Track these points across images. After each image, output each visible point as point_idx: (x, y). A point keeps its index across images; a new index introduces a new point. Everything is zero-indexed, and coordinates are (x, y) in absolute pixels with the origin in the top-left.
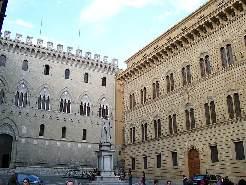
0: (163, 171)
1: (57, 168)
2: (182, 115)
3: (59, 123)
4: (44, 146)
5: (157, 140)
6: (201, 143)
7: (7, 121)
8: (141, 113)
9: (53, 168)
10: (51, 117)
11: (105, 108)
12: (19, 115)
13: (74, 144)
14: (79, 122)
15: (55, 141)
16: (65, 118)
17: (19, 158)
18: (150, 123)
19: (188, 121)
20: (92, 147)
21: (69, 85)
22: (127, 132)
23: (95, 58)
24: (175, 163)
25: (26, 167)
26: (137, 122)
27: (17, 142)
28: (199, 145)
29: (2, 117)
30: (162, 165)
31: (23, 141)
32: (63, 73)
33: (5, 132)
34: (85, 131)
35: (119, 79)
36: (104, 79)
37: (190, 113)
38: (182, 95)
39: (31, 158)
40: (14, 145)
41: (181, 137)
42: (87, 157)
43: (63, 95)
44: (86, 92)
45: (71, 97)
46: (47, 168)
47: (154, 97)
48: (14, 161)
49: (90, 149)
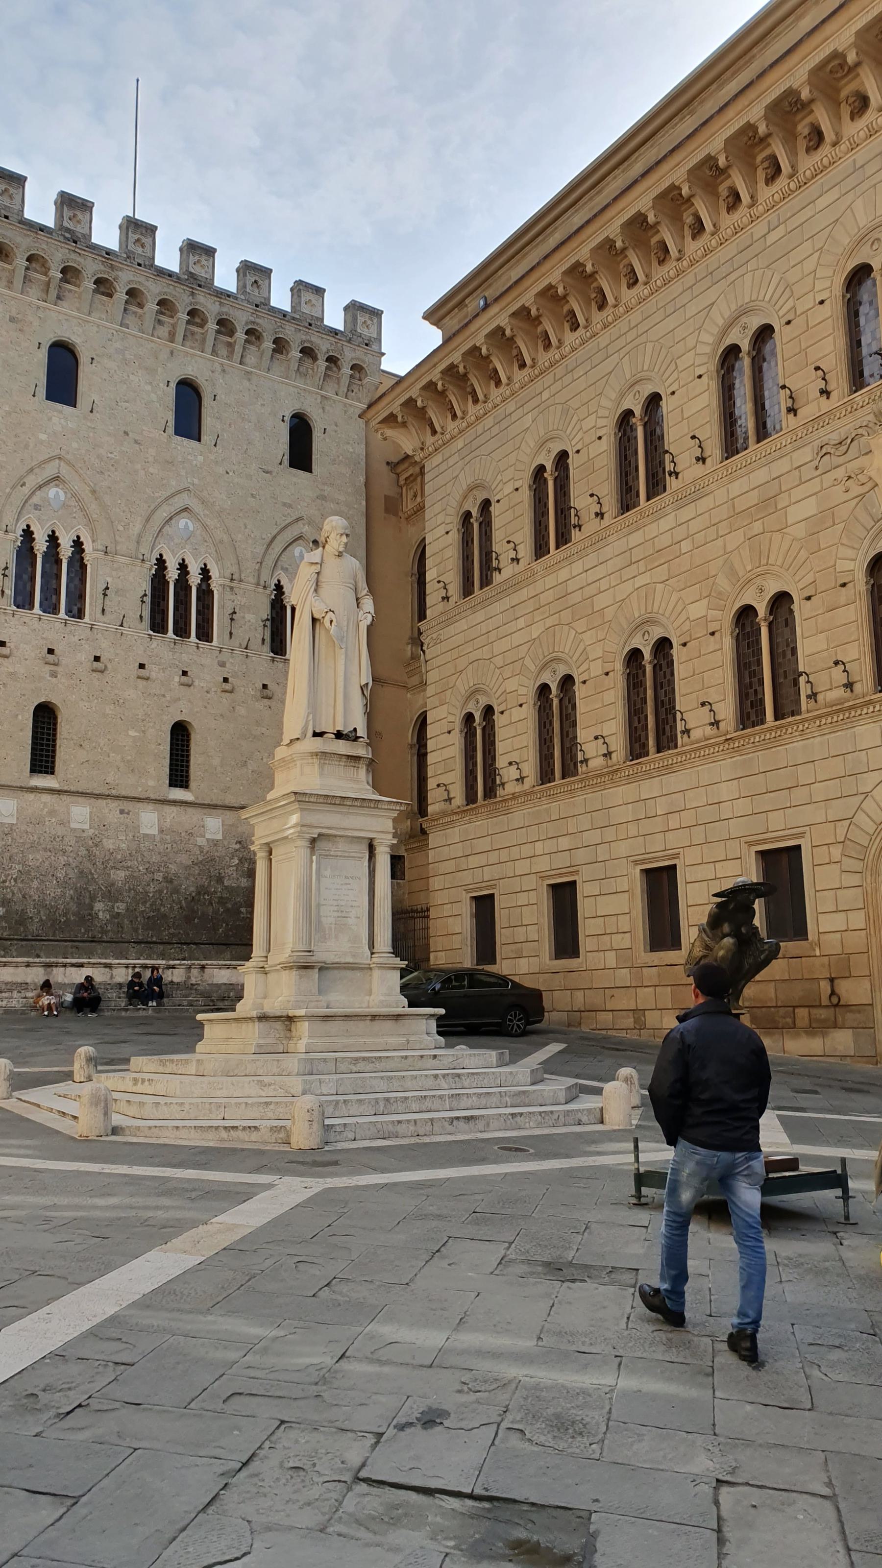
3: (12, 675)
13: (110, 811)
20: (228, 830)
21: (75, 445)
22: (445, 739)
23: (242, 287)
26: (507, 673)
32: (36, 368)
34: (180, 734)
35: (390, 419)
36: (301, 433)
38: (841, 460)
42: (199, 893)
43: (37, 507)
44: (185, 495)
45: (90, 522)
49: (215, 843)
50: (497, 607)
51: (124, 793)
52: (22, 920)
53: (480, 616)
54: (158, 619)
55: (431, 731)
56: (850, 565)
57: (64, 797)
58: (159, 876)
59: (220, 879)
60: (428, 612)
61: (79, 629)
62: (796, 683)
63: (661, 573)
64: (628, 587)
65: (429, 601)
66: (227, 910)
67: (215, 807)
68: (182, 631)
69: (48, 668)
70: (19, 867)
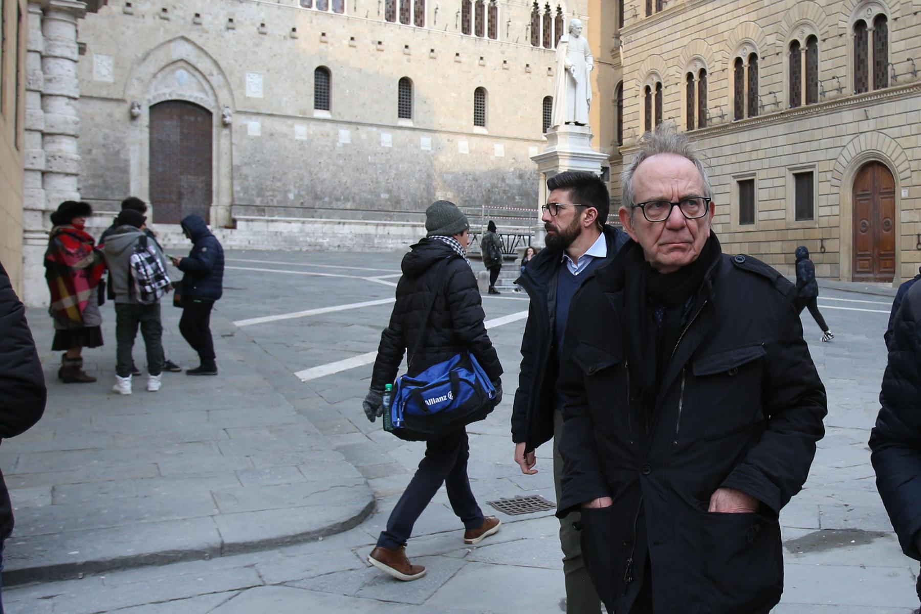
0: (762, 236)
1: (385, 225)
2: (841, 41)
4: (334, 146)
5: (743, 130)
6: (905, 143)
7: (182, 50)
8: (687, 32)
9: (373, 224)
10: (352, 39)
11: (554, 14)
12: (228, 28)
14: (460, 62)
15: (374, 129)
16: (407, 47)
17: (243, 188)
18: (719, 66)
19: (860, 62)
22: (633, 101)
24: (805, 209)
25: (272, 221)
26: (670, 63)
27: (231, 131)
28: (899, 150)
29: (162, 37)
30: (759, 216)
31: (254, 127)
33: (178, 95)
37: (870, 35)
39: (289, 191)
40: (220, 143)
41: (834, 118)
46: (350, 223)
47: (649, 12)
48: (225, 200)
49: (500, 159)
50: (664, 24)
51: (450, 130)
52: (398, 202)
53: (655, 28)
54: (466, 26)
55: (625, 95)
56: (845, 25)
57: (417, 132)
58: (470, 177)
59: (503, 180)
60: (625, 22)
61: (422, 32)
62: (817, 84)
63: (753, 16)
64: (735, 22)
65: (626, 16)
66: (508, 197)
67: (500, 138)
68: (479, 33)
69: (405, 57)
70: (394, 172)
